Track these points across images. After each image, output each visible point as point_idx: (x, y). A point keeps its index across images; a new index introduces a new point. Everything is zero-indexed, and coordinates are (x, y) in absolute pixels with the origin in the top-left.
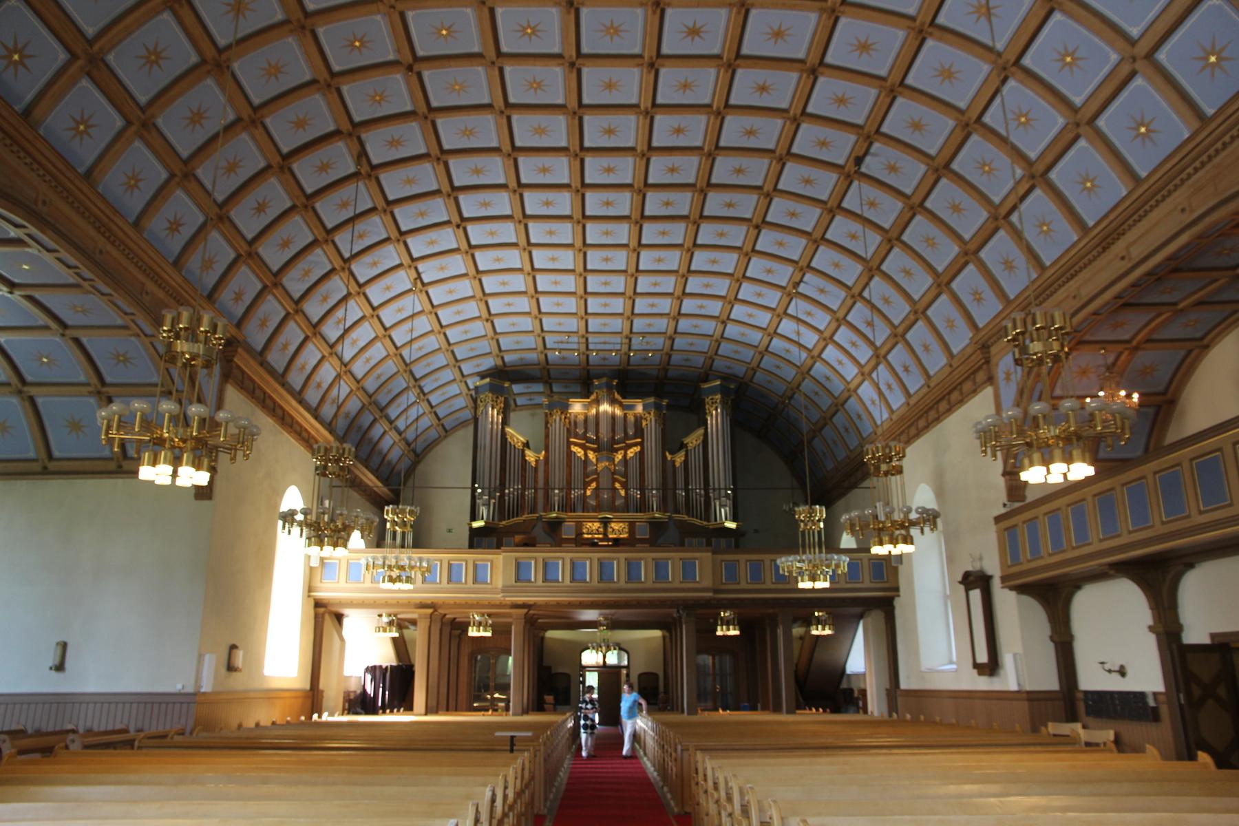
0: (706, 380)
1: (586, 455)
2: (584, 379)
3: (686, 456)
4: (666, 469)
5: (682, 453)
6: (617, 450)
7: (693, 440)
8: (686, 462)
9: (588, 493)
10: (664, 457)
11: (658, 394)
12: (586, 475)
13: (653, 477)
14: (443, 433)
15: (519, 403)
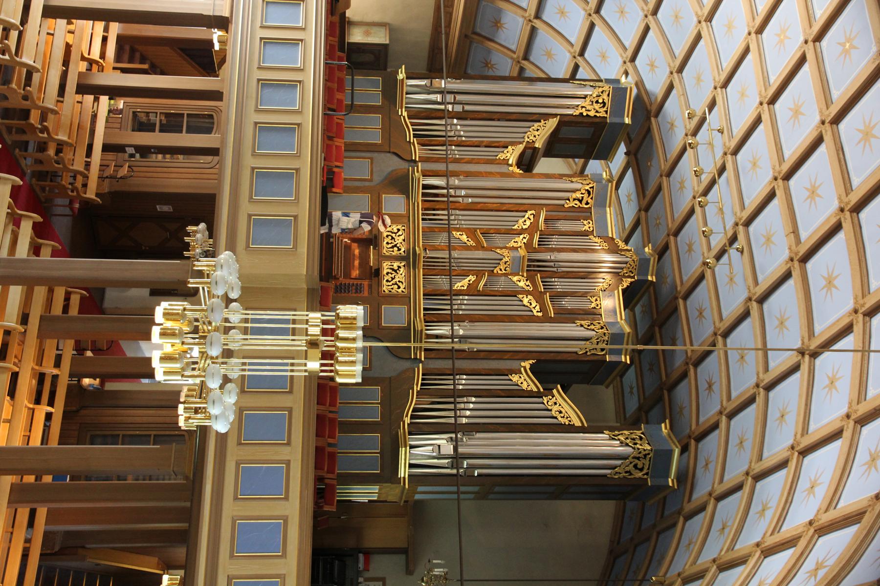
6: (531, 278)
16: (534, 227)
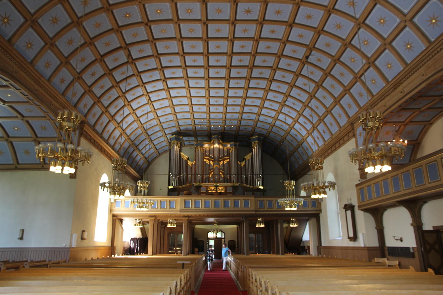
0: (253, 136)
1: (209, 162)
2: (209, 135)
3: (245, 163)
4: (238, 167)
5: (244, 162)
6: (220, 161)
7: (248, 157)
8: (245, 165)
9: (210, 176)
10: (238, 163)
11: (235, 141)
12: (210, 170)
13: (233, 170)
14: (158, 155)
15: (185, 144)
16: (208, 159)
